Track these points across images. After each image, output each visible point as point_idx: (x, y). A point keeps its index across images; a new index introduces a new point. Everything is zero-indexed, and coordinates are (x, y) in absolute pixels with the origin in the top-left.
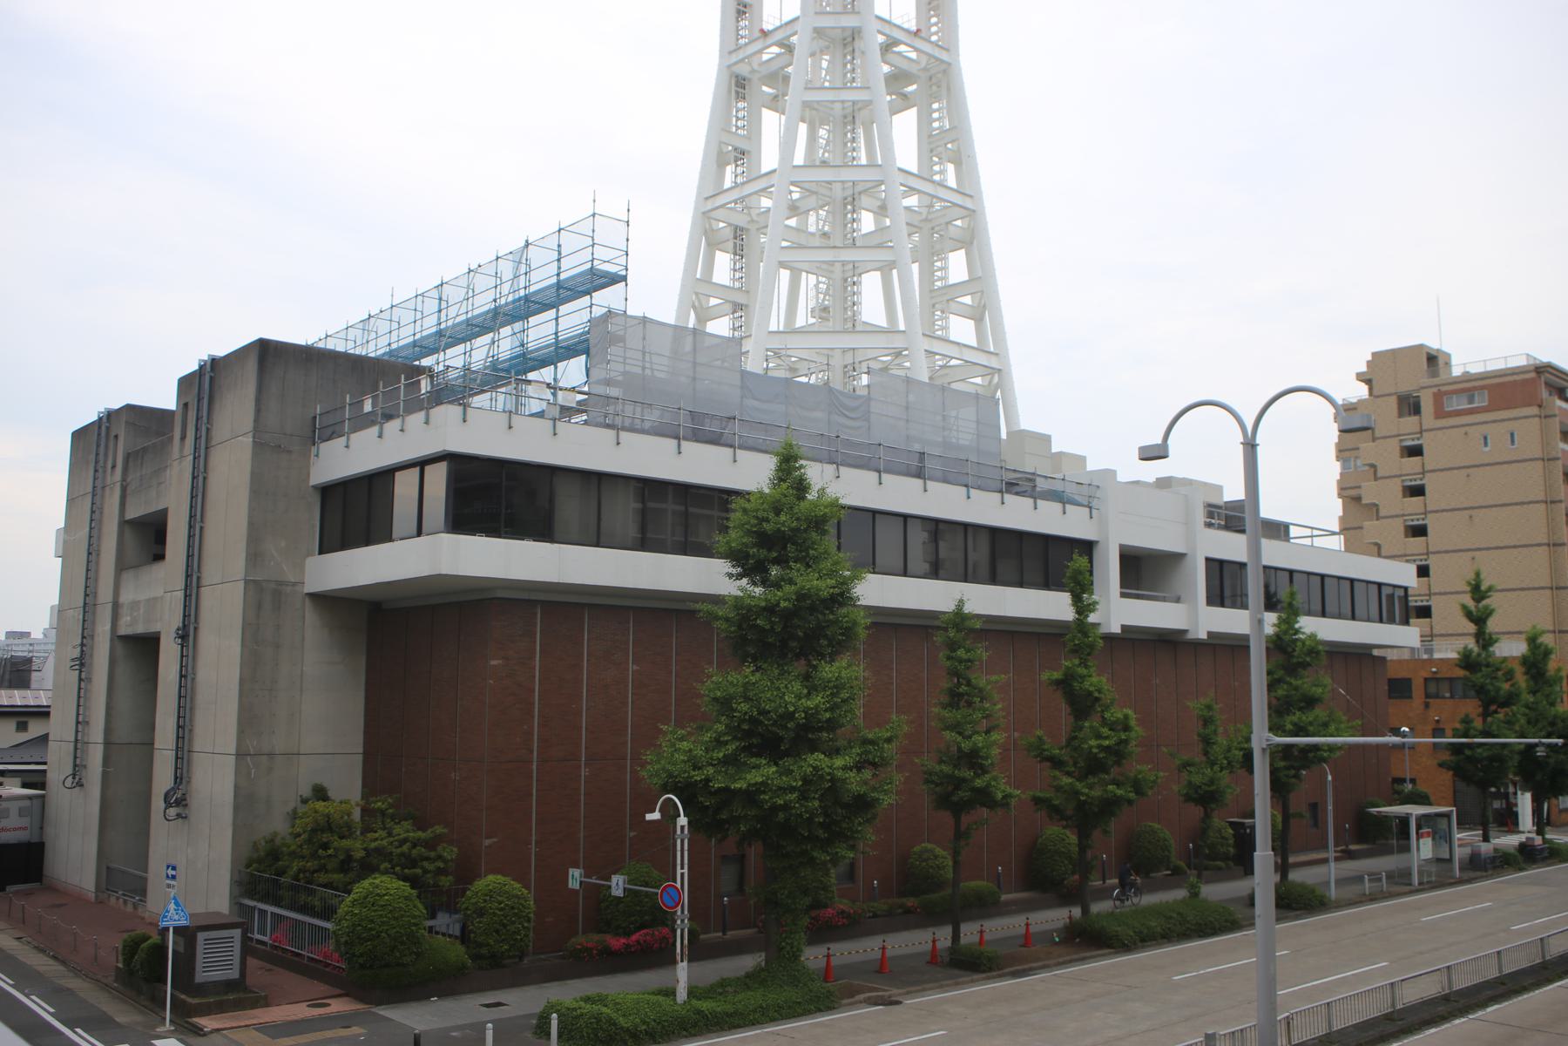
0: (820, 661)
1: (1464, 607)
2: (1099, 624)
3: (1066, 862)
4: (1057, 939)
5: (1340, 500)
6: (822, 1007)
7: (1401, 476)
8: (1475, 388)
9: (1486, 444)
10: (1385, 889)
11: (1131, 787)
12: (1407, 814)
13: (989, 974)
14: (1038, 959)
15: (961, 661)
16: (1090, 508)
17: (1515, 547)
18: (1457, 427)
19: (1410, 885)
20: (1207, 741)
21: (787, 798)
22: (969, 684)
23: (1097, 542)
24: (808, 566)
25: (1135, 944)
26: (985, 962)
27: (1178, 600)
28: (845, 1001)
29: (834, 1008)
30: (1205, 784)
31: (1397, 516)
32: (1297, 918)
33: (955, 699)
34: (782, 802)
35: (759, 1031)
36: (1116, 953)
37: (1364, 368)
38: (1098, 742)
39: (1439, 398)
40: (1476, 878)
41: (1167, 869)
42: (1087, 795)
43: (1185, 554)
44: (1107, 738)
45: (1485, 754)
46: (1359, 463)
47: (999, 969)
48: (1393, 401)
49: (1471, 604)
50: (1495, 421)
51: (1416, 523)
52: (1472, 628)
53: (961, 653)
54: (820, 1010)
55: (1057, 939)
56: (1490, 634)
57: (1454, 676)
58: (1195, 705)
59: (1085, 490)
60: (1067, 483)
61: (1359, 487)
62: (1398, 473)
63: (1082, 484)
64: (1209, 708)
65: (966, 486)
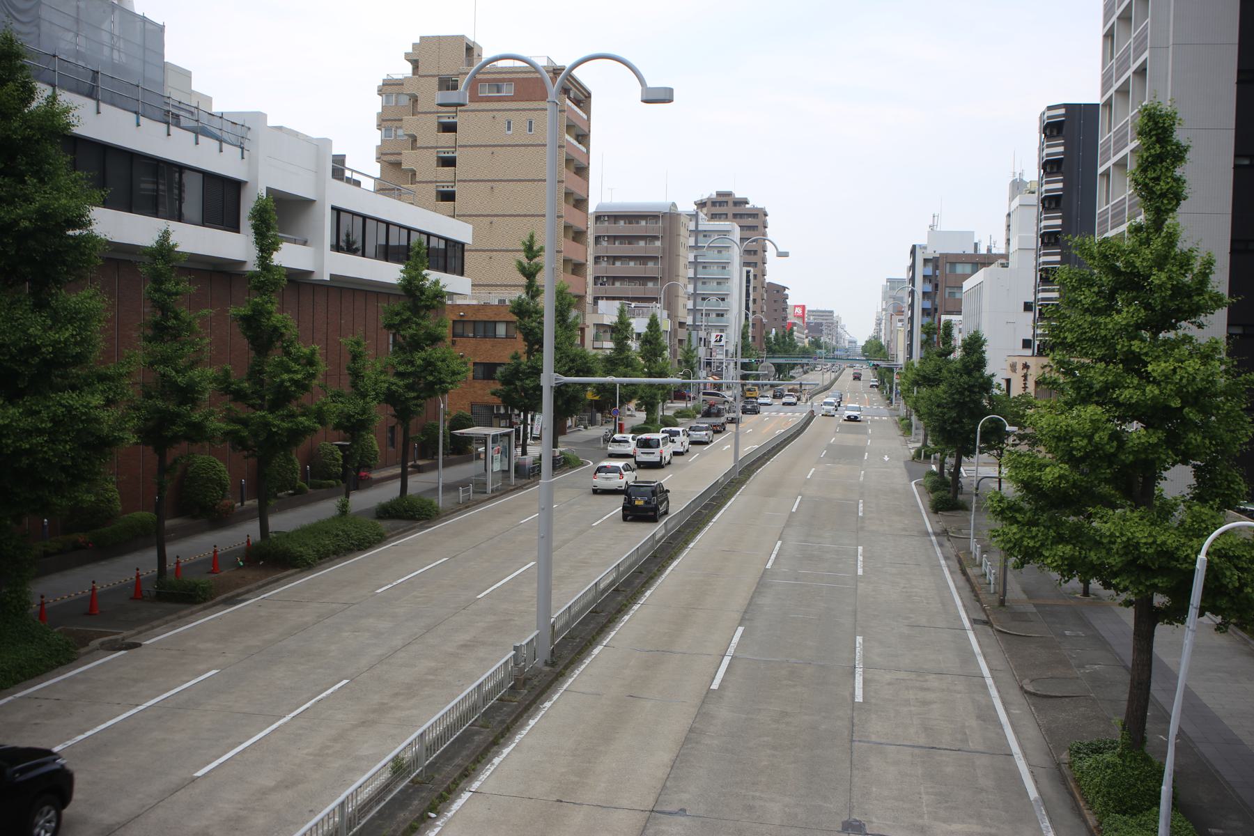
0: (60, 289)
1: (520, 263)
2: (245, 262)
3: (218, 488)
4: (241, 564)
5: (379, 165)
6: (62, 660)
7: (437, 148)
8: (504, 80)
9: (509, 129)
10: (471, 498)
11: (315, 418)
12: (485, 435)
13: (205, 604)
14: (238, 586)
15: (170, 294)
16: (242, 148)
17: (525, 216)
18: (487, 111)
19: (485, 493)
20: (356, 375)
21: (34, 441)
22: (176, 317)
23: (246, 182)
24: (41, 181)
25: (314, 561)
26: (200, 593)
27: (305, 243)
28: (83, 650)
29: (75, 659)
30: (358, 414)
31: (431, 182)
32: (422, 528)
33: (160, 331)
34: (27, 446)
35: (10, 698)
36: (302, 571)
37: (410, 50)
38: (291, 376)
39: (474, 84)
40: (525, 485)
41: (291, 489)
42: (278, 426)
43: (313, 201)
44: (296, 372)
45: (531, 385)
46: (400, 132)
47: (212, 599)
48: (435, 81)
49: (525, 261)
50: (518, 110)
51: (446, 189)
52: (524, 281)
53: (170, 286)
54: (61, 664)
55: (241, 564)
56: (538, 287)
57: (477, 319)
58: (347, 341)
59: (238, 130)
60: (224, 122)
61: (400, 154)
62: (435, 145)
63: (236, 124)
64: (358, 344)
65: (136, 113)
